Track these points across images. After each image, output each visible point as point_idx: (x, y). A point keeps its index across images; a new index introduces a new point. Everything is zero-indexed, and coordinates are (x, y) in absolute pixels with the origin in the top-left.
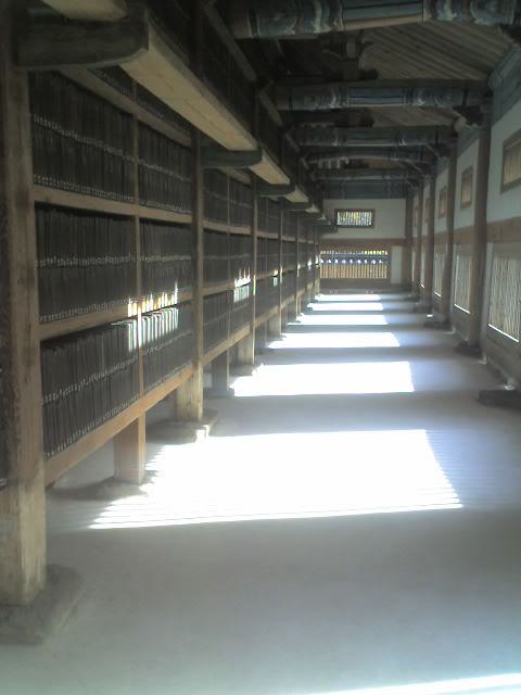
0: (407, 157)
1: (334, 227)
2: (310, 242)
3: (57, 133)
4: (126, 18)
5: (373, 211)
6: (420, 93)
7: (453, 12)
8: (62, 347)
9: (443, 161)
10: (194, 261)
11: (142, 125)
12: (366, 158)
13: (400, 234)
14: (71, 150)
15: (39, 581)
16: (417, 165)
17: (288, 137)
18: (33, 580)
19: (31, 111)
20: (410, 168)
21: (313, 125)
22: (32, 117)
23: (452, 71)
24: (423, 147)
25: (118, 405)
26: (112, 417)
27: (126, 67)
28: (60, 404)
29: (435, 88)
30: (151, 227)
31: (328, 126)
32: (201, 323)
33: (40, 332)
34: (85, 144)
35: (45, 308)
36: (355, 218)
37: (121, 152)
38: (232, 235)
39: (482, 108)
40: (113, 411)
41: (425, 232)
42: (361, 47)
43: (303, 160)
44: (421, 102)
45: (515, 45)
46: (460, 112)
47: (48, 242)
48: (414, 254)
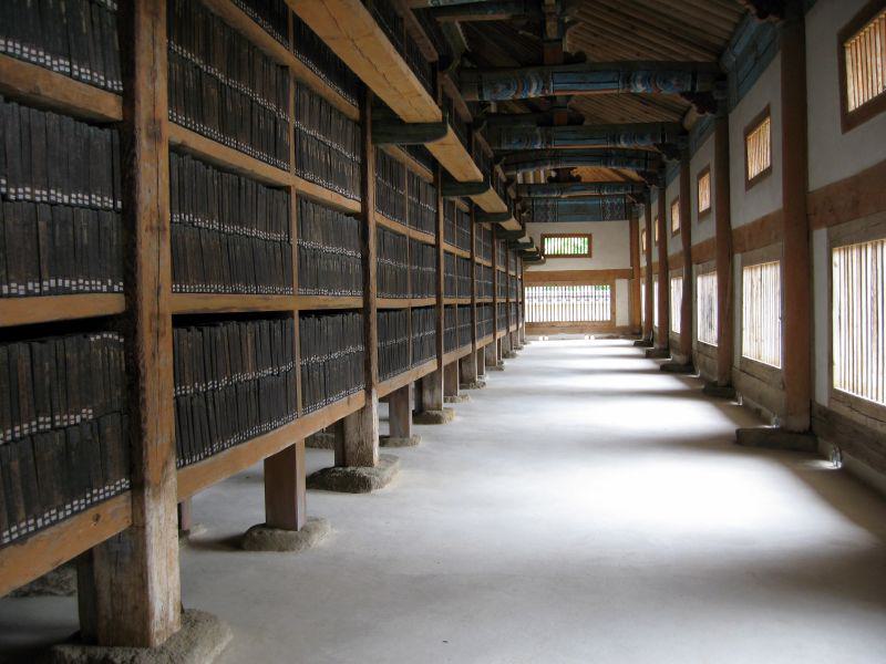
0: (628, 164)
1: (538, 256)
3: (197, 67)
5: (589, 236)
6: (639, 77)
11: (300, 85)
14: (214, 91)
15: (171, 619)
18: (164, 619)
19: (169, 36)
20: (629, 181)
23: (677, 53)
26: (261, 434)
28: (195, 400)
29: (660, 71)
40: (265, 426)
41: (656, 258)
42: (563, 27)
43: (498, 168)
44: (640, 88)
47: (181, 194)
48: (643, 288)
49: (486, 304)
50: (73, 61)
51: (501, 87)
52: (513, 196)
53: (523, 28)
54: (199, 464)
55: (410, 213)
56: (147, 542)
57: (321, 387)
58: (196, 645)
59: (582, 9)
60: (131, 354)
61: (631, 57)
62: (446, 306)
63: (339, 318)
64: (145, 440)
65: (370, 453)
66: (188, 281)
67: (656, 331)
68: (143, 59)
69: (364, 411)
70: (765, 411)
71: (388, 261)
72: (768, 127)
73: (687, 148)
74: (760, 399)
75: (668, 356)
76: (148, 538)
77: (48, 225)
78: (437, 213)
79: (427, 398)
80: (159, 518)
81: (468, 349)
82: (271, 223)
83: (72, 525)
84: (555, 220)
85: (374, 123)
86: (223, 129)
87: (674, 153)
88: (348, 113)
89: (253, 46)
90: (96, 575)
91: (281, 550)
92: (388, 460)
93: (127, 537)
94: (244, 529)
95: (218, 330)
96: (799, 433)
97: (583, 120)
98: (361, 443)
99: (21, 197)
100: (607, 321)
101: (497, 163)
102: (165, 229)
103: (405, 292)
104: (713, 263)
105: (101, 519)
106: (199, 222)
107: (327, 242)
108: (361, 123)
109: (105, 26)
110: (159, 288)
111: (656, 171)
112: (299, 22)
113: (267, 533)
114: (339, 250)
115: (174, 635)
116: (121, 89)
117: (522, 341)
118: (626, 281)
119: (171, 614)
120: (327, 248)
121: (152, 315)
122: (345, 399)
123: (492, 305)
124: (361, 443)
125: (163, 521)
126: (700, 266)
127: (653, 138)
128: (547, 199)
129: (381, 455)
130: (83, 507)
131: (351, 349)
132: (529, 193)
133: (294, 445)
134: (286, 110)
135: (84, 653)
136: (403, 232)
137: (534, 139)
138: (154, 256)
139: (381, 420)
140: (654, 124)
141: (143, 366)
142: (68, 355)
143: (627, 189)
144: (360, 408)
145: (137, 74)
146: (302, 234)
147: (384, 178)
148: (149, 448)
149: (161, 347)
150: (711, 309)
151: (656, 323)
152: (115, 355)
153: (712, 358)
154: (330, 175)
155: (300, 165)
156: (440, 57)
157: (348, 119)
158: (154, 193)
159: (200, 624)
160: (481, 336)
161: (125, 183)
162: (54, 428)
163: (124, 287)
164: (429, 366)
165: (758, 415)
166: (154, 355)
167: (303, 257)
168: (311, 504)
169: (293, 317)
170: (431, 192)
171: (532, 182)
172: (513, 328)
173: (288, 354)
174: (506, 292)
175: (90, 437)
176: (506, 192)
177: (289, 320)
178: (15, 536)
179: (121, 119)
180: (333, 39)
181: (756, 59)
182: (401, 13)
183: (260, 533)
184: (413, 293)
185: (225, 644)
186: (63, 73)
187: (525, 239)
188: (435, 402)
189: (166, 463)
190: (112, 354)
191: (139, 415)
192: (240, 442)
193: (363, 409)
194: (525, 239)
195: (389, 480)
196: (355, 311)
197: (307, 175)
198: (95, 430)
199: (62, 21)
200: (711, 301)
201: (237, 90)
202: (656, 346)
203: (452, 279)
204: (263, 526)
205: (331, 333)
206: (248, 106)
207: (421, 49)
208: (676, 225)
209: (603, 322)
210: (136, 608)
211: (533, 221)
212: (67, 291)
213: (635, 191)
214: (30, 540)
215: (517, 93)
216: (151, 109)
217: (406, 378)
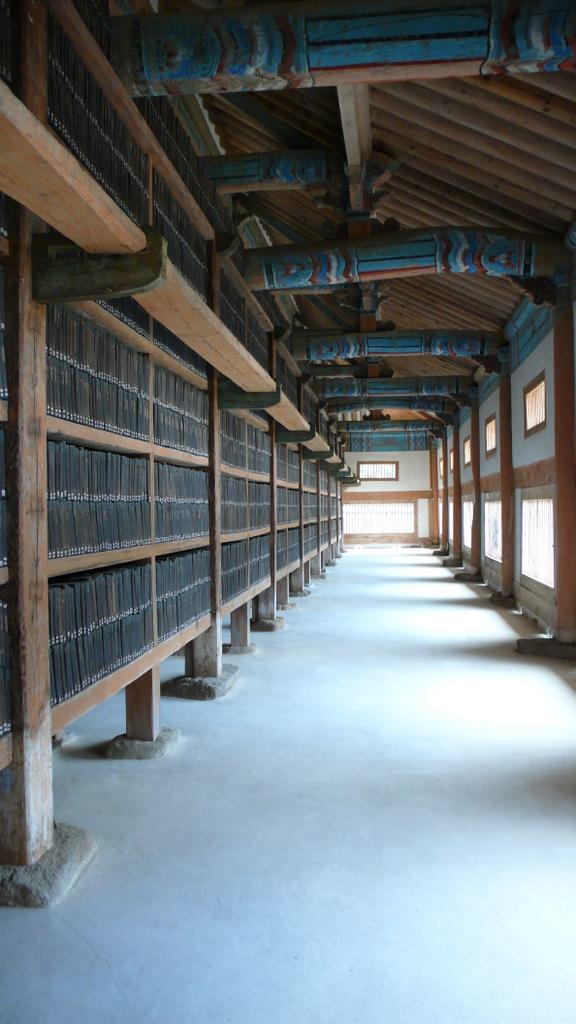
0: (429, 408)
1: (354, 480)
4: (145, 250)
6: (438, 343)
7: (465, 264)
10: (212, 506)
12: (386, 411)
13: (426, 486)
14: (86, 385)
15: (45, 838)
18: (39, 839)
19: (48, 345)
22: (48, 350)
26: (123, 665)
27: (138, 297)
29: (454, 338)
32: (219, 572)
35: (53, 544)
36: (375, 470)
37: (135, 389)
39: (499, 357)
40: (127, 657)
41: (451, 483)
42: (377, 301)
43: (323, 411)
44: (439, 352)
45: (527, 294)
47: (57, 476)
49: (312, 524)
51: (325, 350)
52: (334, 431)
53: (343, 302)
55: (249, 460)
56: (26, 776)
57: (173, 618)
58: (66, 862)
59: (393, 285)
60: (13, 618)
61: (432, 325)
62: (278, 532)
63: (189, 556)
65: (215, 665)
67: (451, 543)
68: (25, 369)
69: (211, 630)
70: (541, 621)
72: (543, 388)
73: (477, 398)
74: (537, 610)
75: (461, 566)
76: (26, 773)
78: (272, 458)
79: (262, 609)
80: (36, 754)
81: (296, 564)
84: (368, 450)
85: (219, 391)
86: (94, 415)
87: (466, 401)
88: (198, 385)
89: (119, 341)
91: (139, 758)
92: (230, 669)
93: (8, 771)
94: (110, 737)
95: (88, 584)
96: (568, 644)
97: (392, 373)
98: (207, 657)
102: (43, 509)
103: (245, 526)
104: (498, 494)
106: (73, 496)
107: (180, 495)
108: (209, 392)
110: (37, 561)
112: (157, 324)
113: (127, 743)
114: (189, 500)
115: (48, 851)
116: (7, 395)
117: (341, 550)
118: (426, 500)
119: (45, 834)
120: (181, 501)
121: (31, 583)
122: (195, 623)
123: (317, 524)
124: (207, 657)
125: (39, 756)
126: (487, 494)
127: (449, 387)
128: (362, 433)
129: (224, 665)
132: (348, 429)
133: (151, 670)
134: (146, 390)
136: (243, 476)
139: (224, 627)
141: (23, 628)
144: (206, 629)
145: (20, 383)
147: (228, 434)
148: (28, 697)
149: (38, 610)
150: (496, 531)
151: (451, 536)
153: (497, 572)
154: (183, 438)
155: (158, 434)
156: (275, 328)
157: (198, 389)
158: (34, 481)
159: (70, 840)
160: (307, 552)
164: (264, 584)
165: (535, 625)
166: (32, 617)
167: (160, 513)
168: (165, 711)
169: (150, 562)
170: (267, 440)
171: (350, 419)
172: (333, 541)
173: (147, 595)
176: (328, 429)
179: (6, 420)
181: (533, 332)
182: (243, 295)
183: (122, 743)
184: (251, 526)
185: (91, 856)
187: (345, 469)
189: (42, 707)
191: (19, 669)
192: (105, 675)
194: (345, 469)
195: (230, 688)
196: (203, 548)
197: (164, 442)
200: (496, 524)
201: (105, 381)
202: (451, 556)
203: (284, 509)
204: (124, 736)
206: (114, 394)
207: (260, 323)
208: (468, 458)
210: (14, 832)
217: (245, 597)
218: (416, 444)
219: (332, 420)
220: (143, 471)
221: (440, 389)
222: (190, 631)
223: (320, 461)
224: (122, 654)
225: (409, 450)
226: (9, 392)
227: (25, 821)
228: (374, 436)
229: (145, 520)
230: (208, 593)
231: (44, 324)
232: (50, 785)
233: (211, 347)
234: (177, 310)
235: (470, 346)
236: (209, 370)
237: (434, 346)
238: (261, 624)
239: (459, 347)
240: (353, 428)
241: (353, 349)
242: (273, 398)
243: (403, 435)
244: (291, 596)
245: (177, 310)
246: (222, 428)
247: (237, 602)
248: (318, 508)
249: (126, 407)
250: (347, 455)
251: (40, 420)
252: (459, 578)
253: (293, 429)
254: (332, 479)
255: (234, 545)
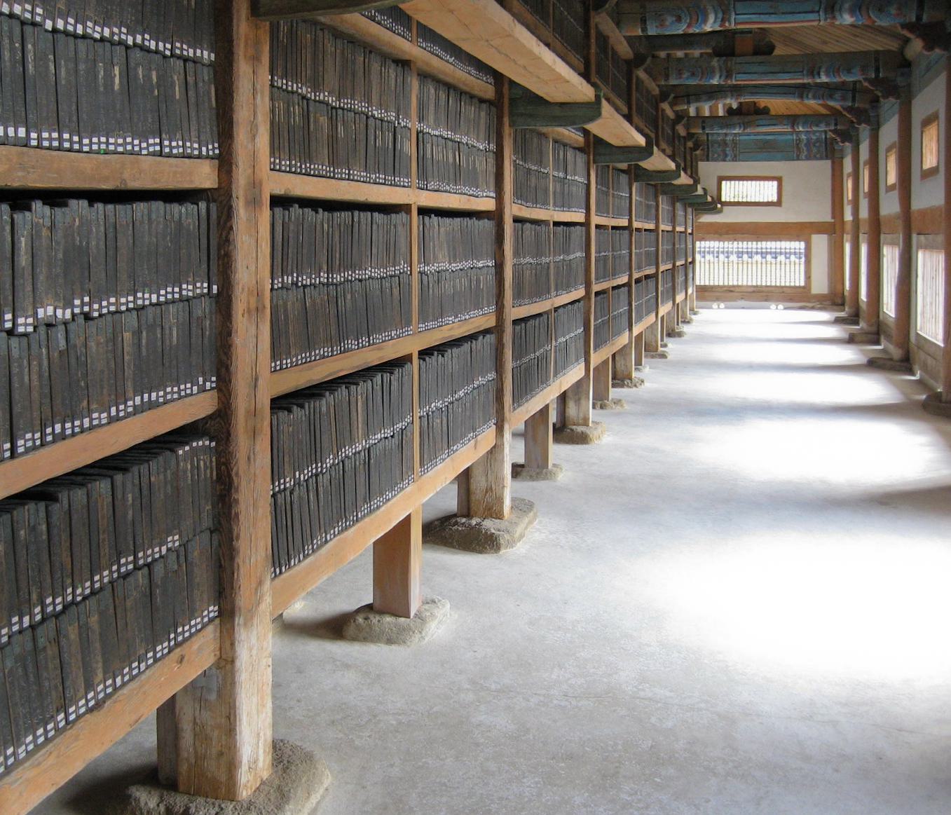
0: (831, 97)
1: (714, 204)
2: (679, 229)
3: (304, 97)
5: (779, 180)
6: (847, 6)
8: (302, 406)
9: (890, 105)
10: (499, 267)
12: (763, 101)
13: (825, 216)
14: (324, 120)
15: (261, 764)
16: (850, 110)
17: (641, 74)
20: (835, 114)
21: (680, 54)
24: (855, 83)
25: (381, 495)
26: (371, 512)
28: (296, 494)
30: (434, 219)
31: (702, 54)
32: (509, 364)
33: (274, 384)
34: (343, 109)
35: (278, 350)
36: (748, 191)
38: (556, 224)
41: (864, 213)
46: (911, 31)
49: (647, 277)
50: (164, 136)
51: (670, 19)
54: (297, 568)
55: (555, 193)
57: (438, 439)
58: (287, 802)
62: (597, 294)
64: (237, 560)
65: (500, 500)
66: (290, 353)
68: (242, 114)
69: (494, 452)
71: (528, 260)
76: (237, 675)
77: (134, 333)
78: (588, 186)
79: (572, 410)
80: (251, 650)
82: (388, 255)
83: (153, 674)
84: (735, 159)
86: (332, 163)
87: (892, 90)
88: (481, 94)
90: (177, 711)
91: (390, 641)
92: (524, 507)
95: (324, 402)
98: (489, 489)
99: (105, 311)
100: (800, 287)
101: (663, 100)
105: (186, 659)
107: (453, 258)
109: (201, 84)
110: (256, 380)
111: (867, 106)
113: (375, 619)
116: (217, 151)
117: (692, 310)
119: (261, 758)
120: (456, 266)
121: (248, 412)
122: (473, 442)
124: (489, 489)
125: (254, 652)
126: (922, 237)
127: (864, 69)
129: (513, 500)
130: (166, 651)
131: (481, 381)
132: (703, 128)
134: (407, 116)
135: (161, 801)
137: (711, 73)
138: (251, 338)
140: (866, 54)
141: (237, 474)
142: (153, 479)
143: (828, 124)
146: (425, 260)
149: (258, 448)
151: (863, 295)
152: (205, 464)
154: (458, 176)
155: (423, 174)
160: (640, 319)
161: (219, 262)
162: (137, 568)
163: (217, 382)
164: (575, 373)
166: (249, 459)
168: (428, 566)
171: (707, 114)
172: (680, 298)
174: (673, 256)
175: (176, 567)
176: (673, 129)
177: (408, 366)
178: (92, 703)
180: (464, 40)
183: (366, 619)
184: (557, 290)
186: (154, 154)
187: (700, 191)
188: (581, 415)
190: (202, 463)
191: (231, 531)
192: (346, 528)
193: (494, 447)
195: (522, 536)
196: (486, 332)
198: (182, 559)
199: (153, 92)
204: (369, 608)
205: (456, 367)
206: (363, 126)
208: (892, 178)
209: (795, 287)
210: (221, 754)
211: (708, 160)
212: (152, 405)
213: (839, 127)
214: (108, 703)
215: (689, 26)
216: (250, 171)
218: (809, 150)
219: (680, 117)
220: (401, 231)
221: (849, 71)
222: (466, 455)
223: (658, 184)
224: (369, 497)
225: (798, 159)
226: (219, 147)
227: (236, 742)
228: (741, 138)
229: (404, 301)
230: (492, 396)
231: (266, 48)
232: (268, 690)
233: (499, 52)
234: (452, 11)
235: (899, 9)
236: (498, 77)
237: (840, 10)
238: (567, 432)
239: (880, 10)
240: (712, 127)
241: (711, 18)
242: (592, 110)
243: (790, 137)
244: (614, 386)
245: (452, 11)
246: (515, 152)
247: (533, 406)
248: (657, 250)
249: (379, 143)
250: (703, 166)
251: (261, 184)
252: (873, 365)
253: (621, 144)
254: (678, 205)
255: (531, 322)
